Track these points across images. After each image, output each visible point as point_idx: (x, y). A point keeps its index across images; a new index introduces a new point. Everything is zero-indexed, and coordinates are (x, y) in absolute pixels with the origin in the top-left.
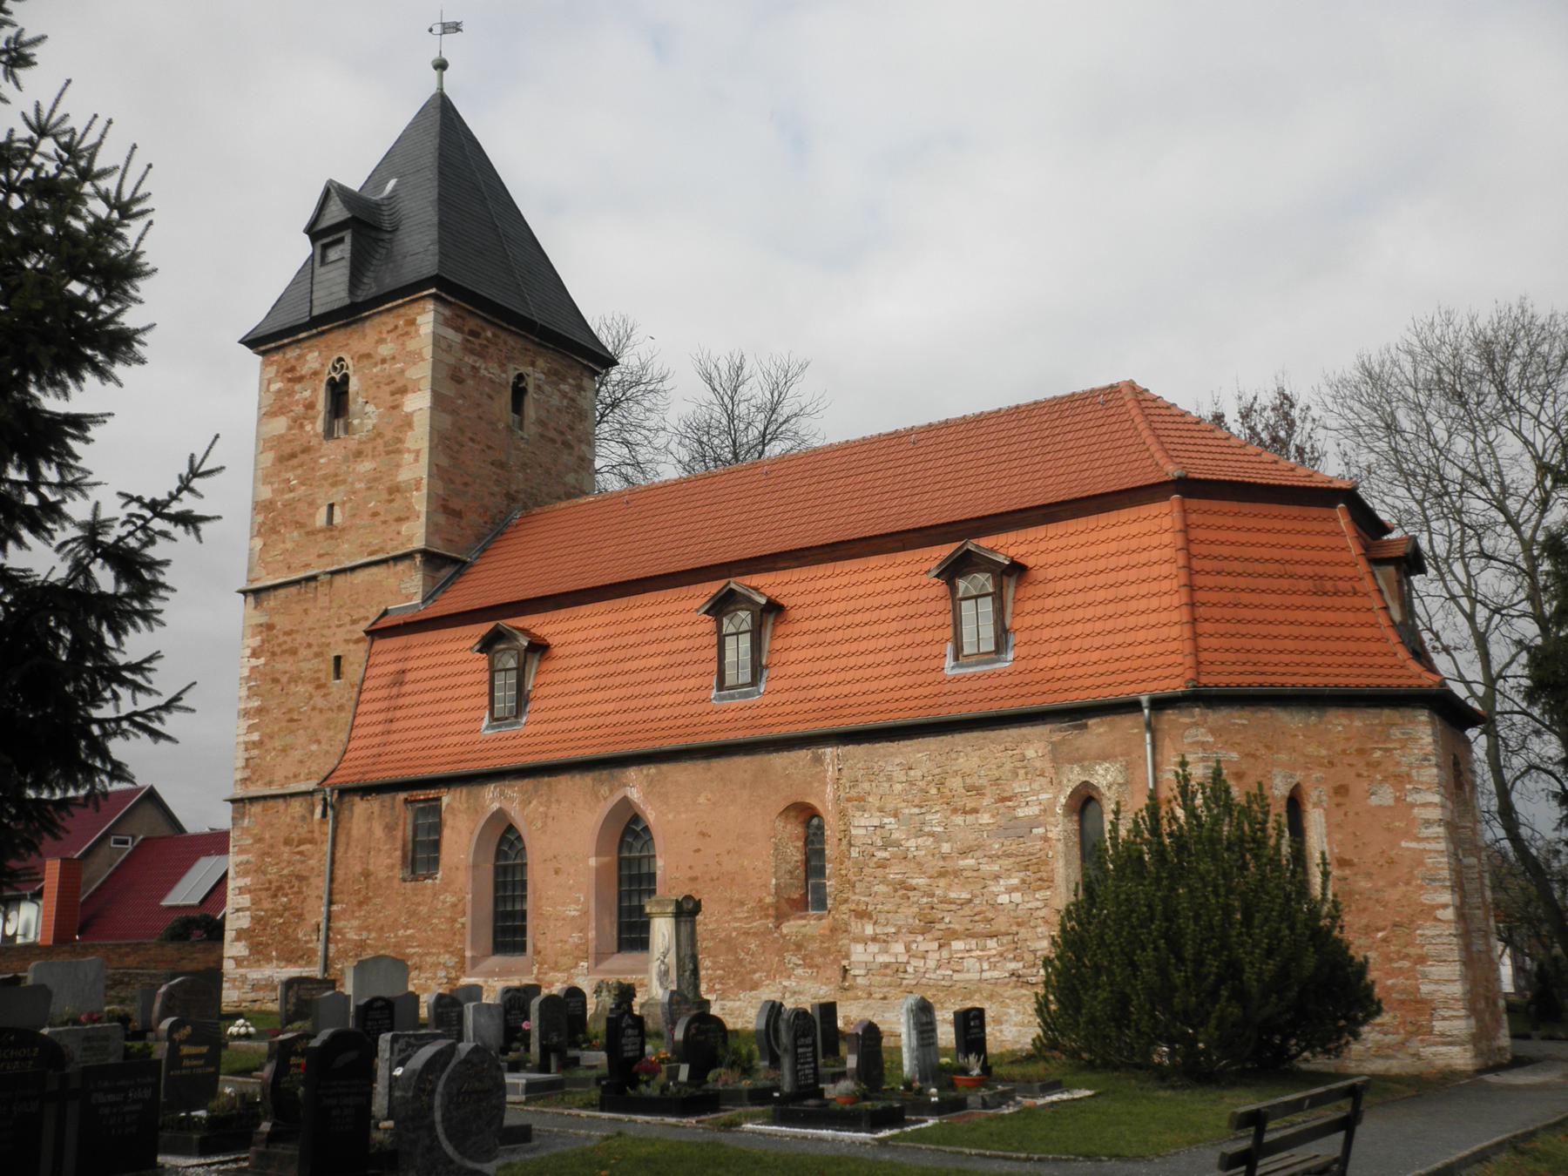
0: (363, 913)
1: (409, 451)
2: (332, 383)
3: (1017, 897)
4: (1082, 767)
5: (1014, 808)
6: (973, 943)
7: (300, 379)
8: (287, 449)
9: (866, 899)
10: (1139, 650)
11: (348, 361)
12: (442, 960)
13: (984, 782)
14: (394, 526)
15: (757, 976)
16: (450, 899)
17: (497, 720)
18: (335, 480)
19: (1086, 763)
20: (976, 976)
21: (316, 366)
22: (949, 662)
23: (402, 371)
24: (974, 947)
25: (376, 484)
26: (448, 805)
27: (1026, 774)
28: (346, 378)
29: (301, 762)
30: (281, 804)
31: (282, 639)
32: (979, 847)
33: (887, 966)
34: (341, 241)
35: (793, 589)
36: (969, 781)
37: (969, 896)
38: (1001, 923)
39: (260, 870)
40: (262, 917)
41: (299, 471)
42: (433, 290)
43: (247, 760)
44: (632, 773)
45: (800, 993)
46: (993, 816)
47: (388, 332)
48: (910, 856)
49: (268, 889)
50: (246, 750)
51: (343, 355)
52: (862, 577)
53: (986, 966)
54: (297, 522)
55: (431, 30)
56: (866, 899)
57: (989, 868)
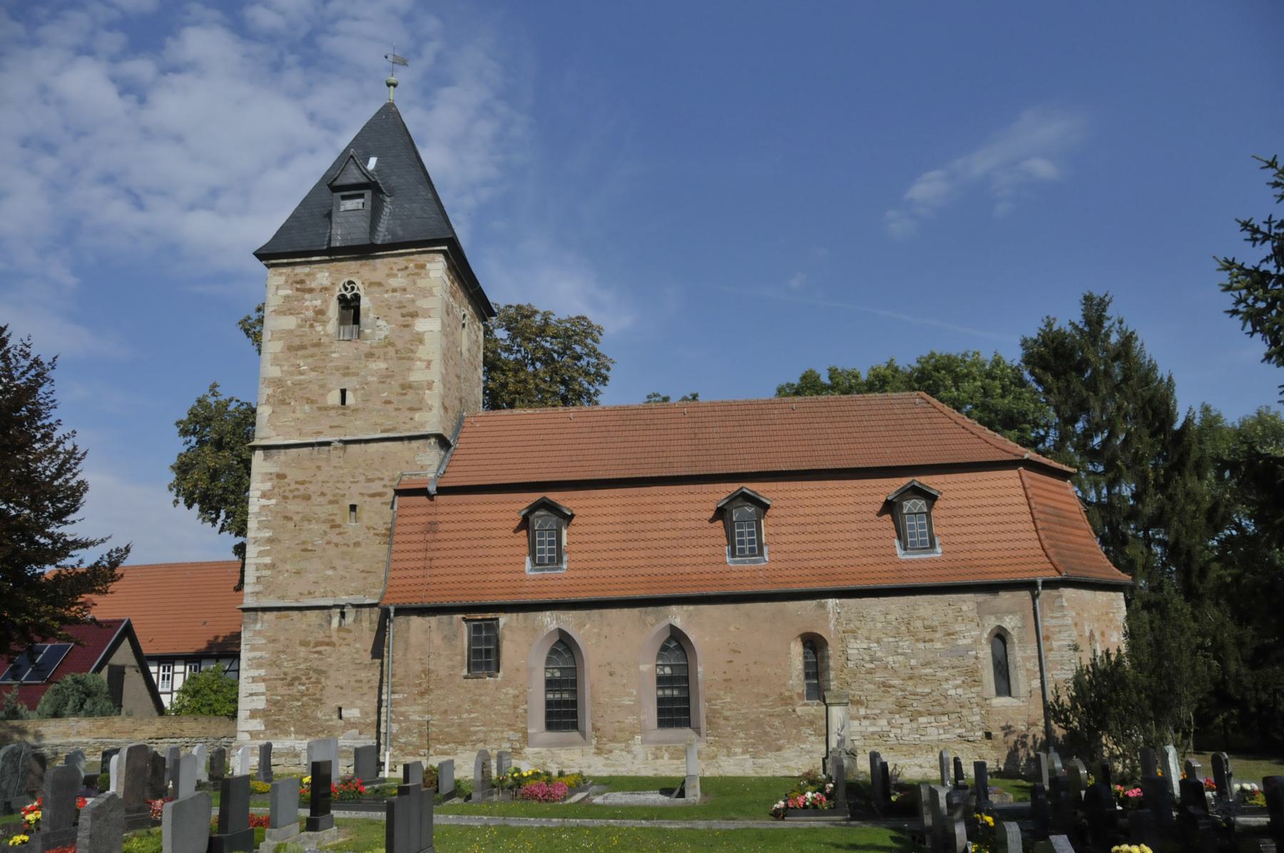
0: (426, 701)
1: (420, 360)
2: (342, 299)
3: (960, 691)
4: (996, 617)
5: (956, 639)
6: (932, 719)
7: (311, 291)
8: (297, 342)
9: (860, 693)
10: (1020, 553)
11: (358, 284)
12: (505, 735)
13: (936, 623)
14: (410, 414)
15: (782, 742)
16: (511, 691)
17: (538, 565)
18: (346, 372)
19: (999, 615)
20: (935, 738)
21: (326, 283)
22: (899, 551)
23: (413, 301)
24: (933, 721)
25: (389, 380)
26: (505, 624)
27: (963, 620)
28: (357, 298)
29: (316, 583)
30: (295, 614)
31: (293, 486)
32: (935, 662)
33: (873, 733)
34: (361, 196)
35: (774, 495)
36: (926, 622)
37: (930, 691)
38: (950, 706)
39: (273, 664)
40: (278, 701)
41: (310, 360)
42: (445, 248)
43: (258, 578)
44: (674, 608)
45: (813, 752)
46: (943, 644)
47: (399, 270)
48: (889, 667)
49: (283, 679)
50: (257, 570)
51: (353, 279)
52: (837, 492)
53: (941, 731)
54: (308, 399)
55: (386, 57)
56: (860, 693)
57: (940, 674)
